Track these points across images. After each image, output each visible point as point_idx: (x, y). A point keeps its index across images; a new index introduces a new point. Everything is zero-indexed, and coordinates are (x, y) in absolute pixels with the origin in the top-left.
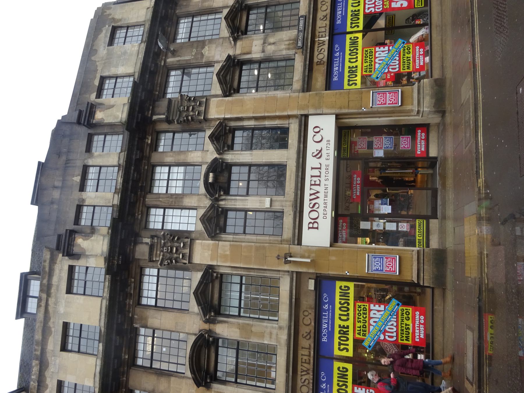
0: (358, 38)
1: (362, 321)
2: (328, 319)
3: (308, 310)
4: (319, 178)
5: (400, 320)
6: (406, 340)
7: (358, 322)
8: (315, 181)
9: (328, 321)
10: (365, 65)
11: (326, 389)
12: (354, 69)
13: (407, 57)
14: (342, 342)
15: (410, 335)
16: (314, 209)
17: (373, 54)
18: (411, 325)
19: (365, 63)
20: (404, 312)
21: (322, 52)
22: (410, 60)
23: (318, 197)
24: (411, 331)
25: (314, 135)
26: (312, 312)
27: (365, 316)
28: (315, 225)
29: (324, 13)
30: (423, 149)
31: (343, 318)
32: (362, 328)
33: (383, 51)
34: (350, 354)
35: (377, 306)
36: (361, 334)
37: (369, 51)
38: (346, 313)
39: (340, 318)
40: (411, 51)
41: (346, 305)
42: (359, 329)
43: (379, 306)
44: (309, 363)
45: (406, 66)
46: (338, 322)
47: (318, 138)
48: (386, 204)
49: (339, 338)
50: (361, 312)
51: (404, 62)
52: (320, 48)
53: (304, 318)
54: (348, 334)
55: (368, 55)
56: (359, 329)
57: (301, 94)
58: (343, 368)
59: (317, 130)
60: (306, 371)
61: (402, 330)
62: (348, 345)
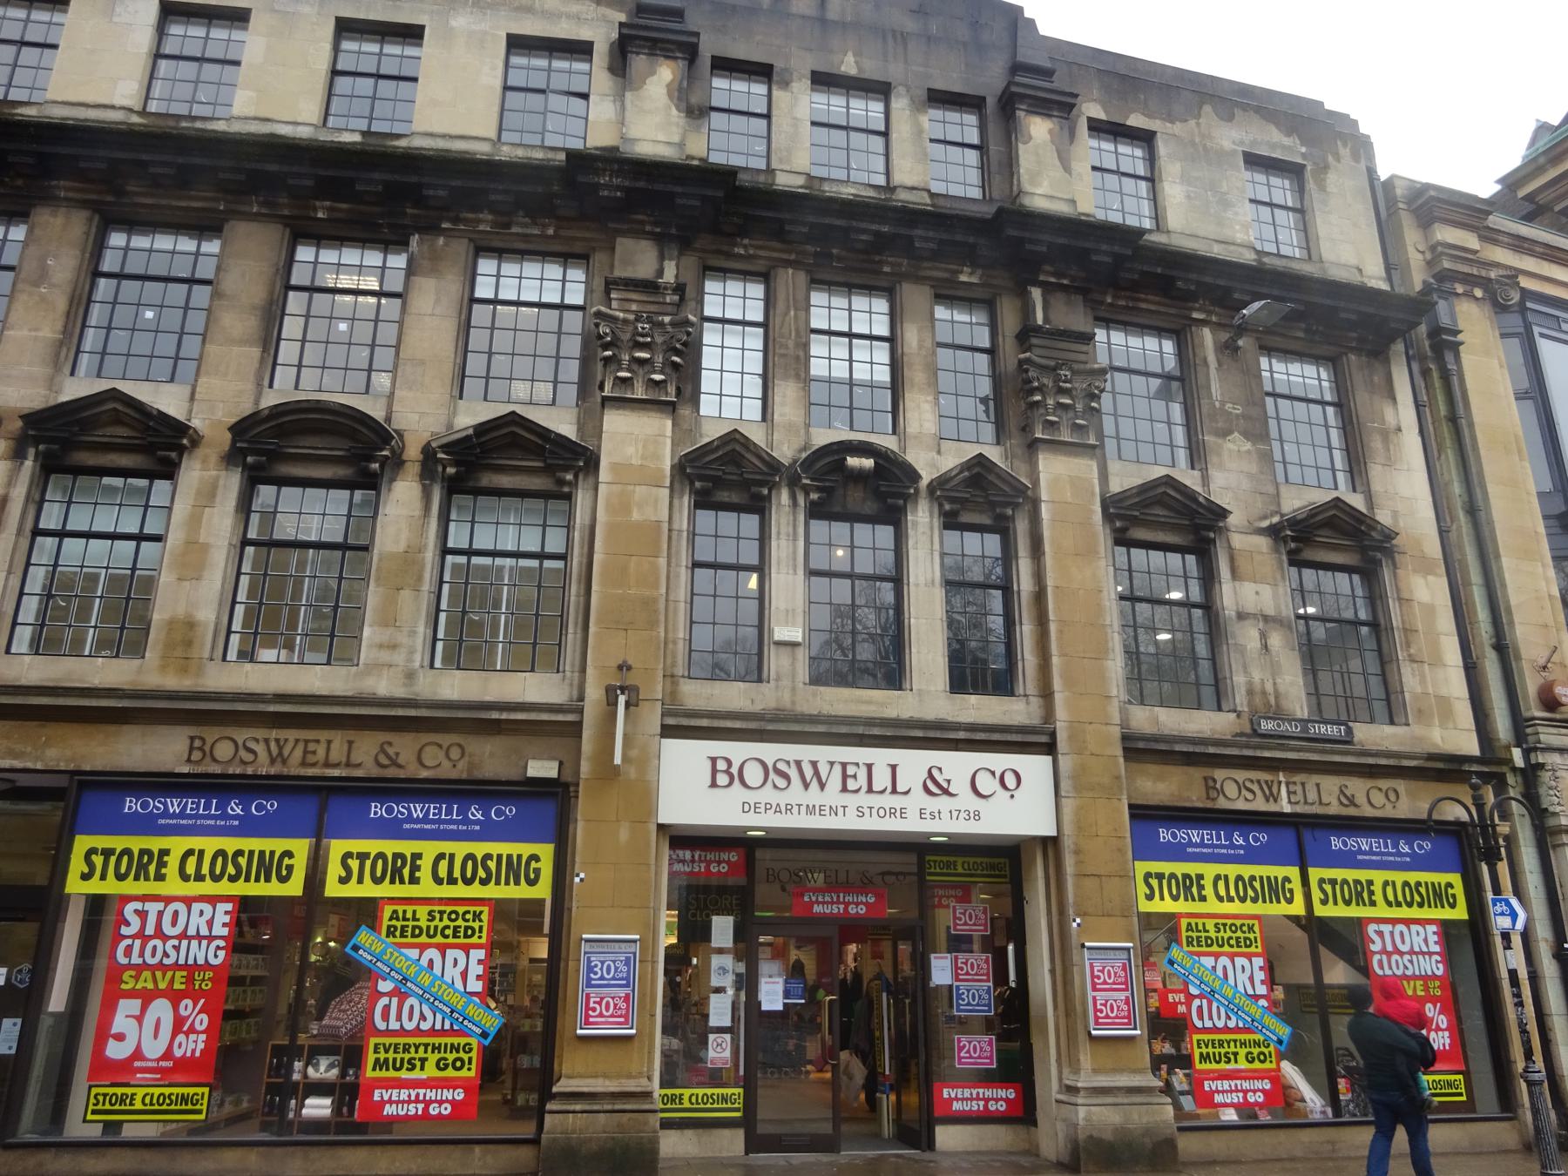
1: (432, 924)
2: (440, 821)
3: (466, 758)
4: (865, 788)
5: (436, 1041)
6: (377, 1060)
7: (430, 913)
8: (855, 776)
9: (190, 817)
10: (422, 911)
11: (466, 821)
12: (1194, 890)
13: (1236, 1054)
14: (368, 863)
15: (392, 1074)
16: (772, 775)
18: (424, 1075)
19: (1216, 925)
20: (462, 1054)
21: (1244, 792)
22: (1229, 1061)
23: (806, 786)
24: (404, 1074)
25: (993, 773)
26: (460, 772)
27: (447, 932)
28: (722, 779)
29: (1361, 799)
30: (956, 1106)
31: (192, 861)
32: (411, 923)
33: (1251, 979)
34: (333, 889)
35: (480, 970)
36: (394, 922)
37: (1251, 936)
38: (457, 873)
39: (441, 856)
40: (1257, 1065)
41: (481, 873)
42: (409, 915)
43: (479, 977)
44: (304, 764)
45: (1210, 1050)
46: (429, 849)
47: (986, 784)
48: (787, 994)
49: (381, 855)
50: (460, 922)
51: (1221, 1045)
52: (1255, 787)
53: (440, 746)
54: (392, 882)
56: (409, 915)
57: (1116, 732)
58: (290, 868)
59: (1010, 781)
60: (280, 754)
61: (406, 1049)
62: (103, 877)
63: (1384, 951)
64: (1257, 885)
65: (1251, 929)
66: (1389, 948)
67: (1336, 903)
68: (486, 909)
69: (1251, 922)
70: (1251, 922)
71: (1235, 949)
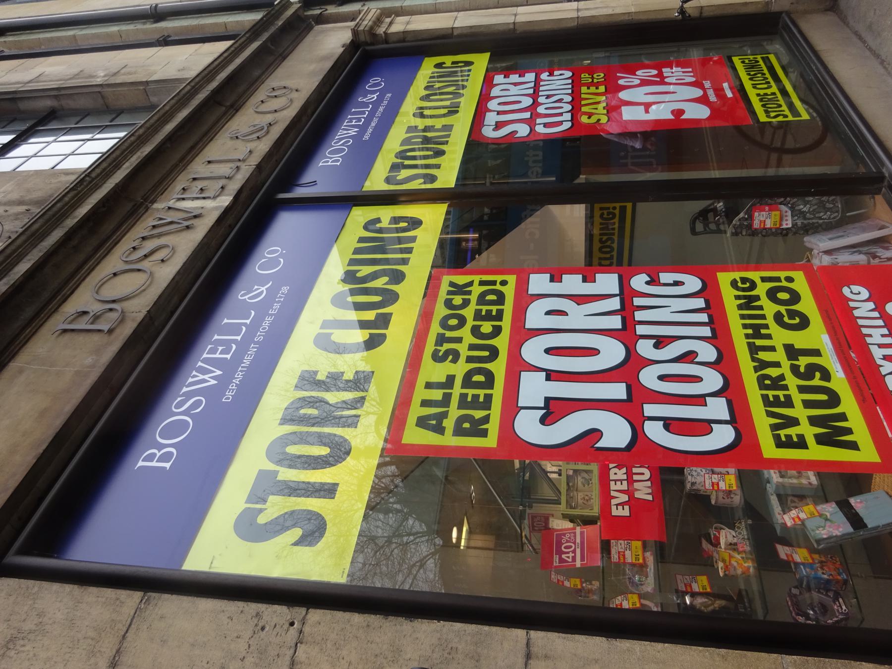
0: (416, 223)
1: (464, 351)
6: (821, 440)
12: (333, 397)
17: (508, 308)
19: (437, 358)
33: (581, 299)
36: (449, 424)
37: (477, 290)
42: (437, 395)
51: (778, 383)
55: (468, 313)
56: (437, 395)
63: (531, 122)
64: (365, 270)
65: (458, 289)
66: (527, 115)
67: (329, 491)
68: (446, 280)
69: (444, 287)
70: (444, 287)
71: (506, 323)
